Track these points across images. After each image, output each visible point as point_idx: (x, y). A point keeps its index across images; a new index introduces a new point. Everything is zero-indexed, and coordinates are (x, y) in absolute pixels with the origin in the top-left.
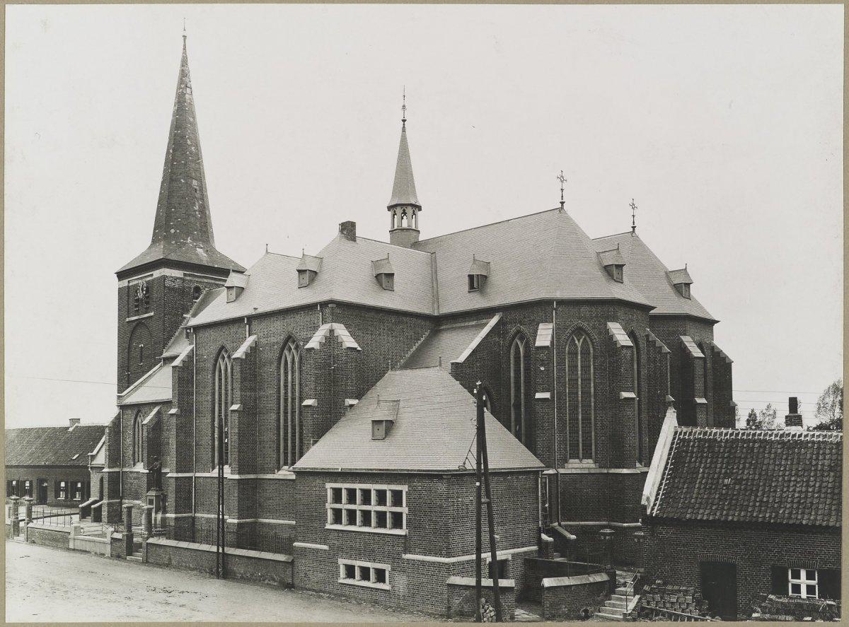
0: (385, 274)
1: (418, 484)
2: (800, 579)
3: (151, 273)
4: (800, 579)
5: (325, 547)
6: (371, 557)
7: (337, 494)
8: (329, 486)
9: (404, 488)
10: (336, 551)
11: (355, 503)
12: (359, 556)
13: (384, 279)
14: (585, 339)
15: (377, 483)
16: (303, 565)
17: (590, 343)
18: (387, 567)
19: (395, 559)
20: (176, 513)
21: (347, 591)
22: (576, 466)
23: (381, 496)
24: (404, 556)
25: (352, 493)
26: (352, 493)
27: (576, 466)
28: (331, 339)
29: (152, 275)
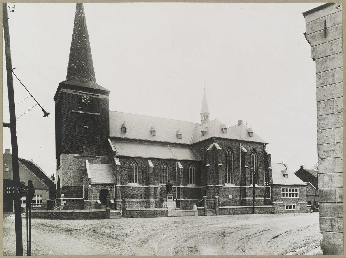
0: (224, 128)
1: (300, 187)
2: (169, 199)
3: (98, 95)
4: (169, 199)
5: (282, 202)
6: (292, 203)
7: (283, 190)
8: (282, 188)
9: (298, 188)
10: (284, 203)
11: (293, 194)
12: (290, 203)
13: (224, 130)
14: (136, 164)
15: (285, 187)
16: (276, 208)
17: (137, 166)
18: (296, 205)
19: (297, 203)
20: (245, 200)
21: (287, 211)
22: (190, 186)
23: (287, 190)
24: (299, 202)
25: (290, 190)
26: (287, 190)
27: (190, 186)
28: (214, 147)
29: (98, 96)
